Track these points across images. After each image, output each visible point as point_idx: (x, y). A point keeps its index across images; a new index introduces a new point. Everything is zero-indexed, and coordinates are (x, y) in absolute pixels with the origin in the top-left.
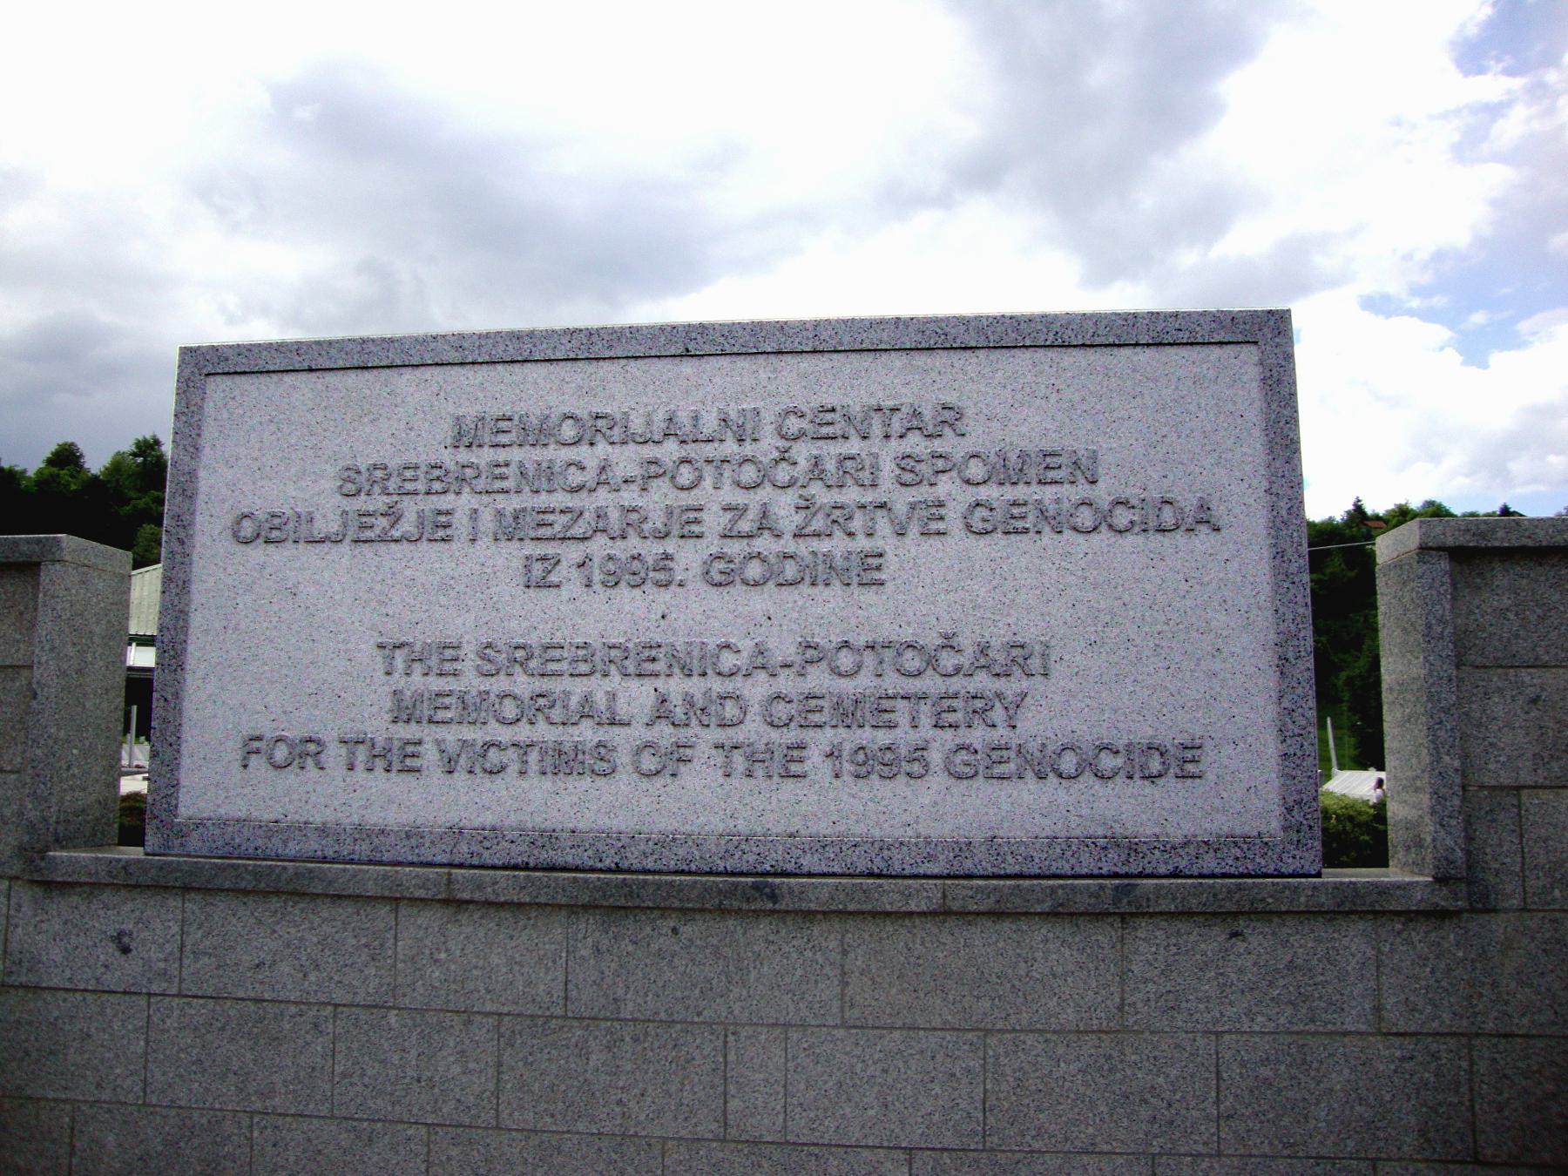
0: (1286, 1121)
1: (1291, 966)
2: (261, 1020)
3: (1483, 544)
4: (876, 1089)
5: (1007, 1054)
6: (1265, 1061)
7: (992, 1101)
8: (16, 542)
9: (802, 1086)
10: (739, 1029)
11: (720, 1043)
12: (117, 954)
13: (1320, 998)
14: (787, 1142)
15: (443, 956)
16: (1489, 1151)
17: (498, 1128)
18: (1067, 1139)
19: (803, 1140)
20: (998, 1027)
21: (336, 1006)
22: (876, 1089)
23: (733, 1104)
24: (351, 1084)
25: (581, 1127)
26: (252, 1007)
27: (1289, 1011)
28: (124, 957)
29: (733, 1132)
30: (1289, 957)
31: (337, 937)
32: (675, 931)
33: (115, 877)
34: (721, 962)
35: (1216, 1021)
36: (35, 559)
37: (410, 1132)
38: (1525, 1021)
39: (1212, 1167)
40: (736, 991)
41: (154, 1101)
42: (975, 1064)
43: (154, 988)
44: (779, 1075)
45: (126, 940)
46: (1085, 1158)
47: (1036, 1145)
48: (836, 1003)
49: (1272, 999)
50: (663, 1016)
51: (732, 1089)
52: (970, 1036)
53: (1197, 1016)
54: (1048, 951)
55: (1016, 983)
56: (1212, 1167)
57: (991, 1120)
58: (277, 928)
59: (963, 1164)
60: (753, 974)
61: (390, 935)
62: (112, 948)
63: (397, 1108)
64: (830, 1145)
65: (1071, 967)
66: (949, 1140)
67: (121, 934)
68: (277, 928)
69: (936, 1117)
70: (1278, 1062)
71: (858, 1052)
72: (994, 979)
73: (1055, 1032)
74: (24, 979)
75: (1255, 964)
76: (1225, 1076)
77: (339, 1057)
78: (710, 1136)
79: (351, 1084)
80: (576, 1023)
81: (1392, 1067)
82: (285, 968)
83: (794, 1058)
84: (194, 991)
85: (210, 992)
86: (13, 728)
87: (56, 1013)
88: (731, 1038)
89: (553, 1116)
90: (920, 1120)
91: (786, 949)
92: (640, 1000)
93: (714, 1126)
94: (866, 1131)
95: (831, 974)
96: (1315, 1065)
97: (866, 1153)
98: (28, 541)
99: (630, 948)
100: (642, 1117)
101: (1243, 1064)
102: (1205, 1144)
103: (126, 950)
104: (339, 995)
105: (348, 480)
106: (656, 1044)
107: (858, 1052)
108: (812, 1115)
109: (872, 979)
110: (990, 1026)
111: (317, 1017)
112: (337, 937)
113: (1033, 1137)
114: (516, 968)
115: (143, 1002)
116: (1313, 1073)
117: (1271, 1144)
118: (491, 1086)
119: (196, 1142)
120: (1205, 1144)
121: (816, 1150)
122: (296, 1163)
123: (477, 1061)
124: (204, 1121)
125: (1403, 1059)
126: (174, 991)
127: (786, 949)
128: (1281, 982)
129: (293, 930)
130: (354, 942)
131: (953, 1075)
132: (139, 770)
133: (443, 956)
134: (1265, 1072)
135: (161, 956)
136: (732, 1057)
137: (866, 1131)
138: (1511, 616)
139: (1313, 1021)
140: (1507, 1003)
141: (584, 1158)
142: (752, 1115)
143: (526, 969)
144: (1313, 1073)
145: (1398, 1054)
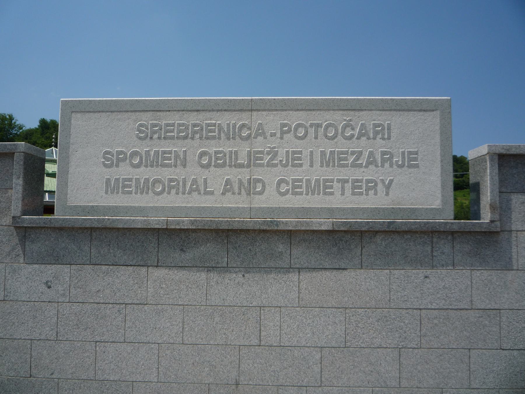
0: (442, 337)
1: (444, 287)
2: (99, 309)
3: (508, 153)
4: (310, 327)
5: (353, 316)
6: (436, 318)
7: (347, 331)
8: (5, 145)
9: (286, 327)
10: (265, 308)
11: (258, 313)
12: (46, 288)
13: (453, 298)
14: (281, 346)
15: (164, 286)
16: (505, 345)
17: (183, 344)
18: (372, 343)
19: (286, 345)
20: (350, 307)
21: (126, 304)
22: (310, 327)
23: (263, 334)
24: (132, 331)
25: (211, 342)
26: (96, 305)
27: (443, 301)
28: (48, 290)
29: (263, 343)
30: (443, 284)
31: (126, 280)
32: (244, 276)
33: (46, 224)
34: (259, 286)
35: (420, 305)
36: (13, 151)
37: (152, 346)
38: (517, 305)
39: (418, 352)
40: (264, 296)
41: (61, 338)
42: (342, 319)
43: (60, 300)
44: (278, 323)
45: (49, 284)
46: (378, 349)
47: (363, 345)
48: (297, 299)
49: (438, 298)
50: (239, 304)
51: (262, 328)
52: (341, 309)
53: (414, 303)
54: (366, 282)
55: (356, 292)
56: (418, 352)
57: (348, 338)
58: (105, 278)
59: (339, 351)
60: (270, 289)
61: (145, 280)
62: (44, 286)
63: (148, 338)
64: (295, 347)
65: (373, 287)
66: (334, 344)
67: (47, 282)
68: (105, 278)
69: (330, 337)
70: (440, 318)
71: (304, 315)
72: (349, 291)
73: (368, 308)
74: (11, 298)
75: (433, 286)
76: (423, 323)
77: (127, 322)
78: (255, 344)
79: (132, 331)
80: (210, 307)
81: (476, 320)
82: (108, 291)
83: (283, 317)
84: (75, 300)
85: (80, 300)
86: (5, 210)
87: (24, 310)
88: (262, 311)
89: (202, 339)
90: (324, 337)
91: (280, 281)
92: (232, 299)
93: (257, 341)
94: (307, 341)
95: (295, 289)
96: (452, 319)
97: (307, 349)
98: (10, 145)
99: (229, 281)
100: (233, 338)
101: (429, 319)
102: (417, 345)
103: (49, 287)
104: (127, 301)
105: (141, 131)
106: (237, 314)
107: (304, 315)
108: (289, 336)
109: (309, 291)
110: (347, 307)
111: (119, 308)
112: (126, 280)
113: (361, 343)
114: (189, 289)
115: (56, 305)
116: (451, 322)
117: (437, 344)
118: (181, 329)
119: (76, 352)
120: (417, 345)
121: (290, 348)
122: (112, 358)
123: (176, 321)
124: (79, 345)
125: (479, 317)
126: (68, 301)
127: (280, 281)
128: (441, 293)
129: (110, 279)
130: (132, 282)
131: (335, 323)
132: (54, 161)
133: (164, 286)
134: (436, 321)
135: (62, 289)
136: (262, 318)
137: (307, 341)
138: (516, 176)
139: (451, 305)
140: (512, 299)
141: (212, 353)
142: (269, 337)
143: (192, 290)
144: (451, 322)
145: (478, 315)
